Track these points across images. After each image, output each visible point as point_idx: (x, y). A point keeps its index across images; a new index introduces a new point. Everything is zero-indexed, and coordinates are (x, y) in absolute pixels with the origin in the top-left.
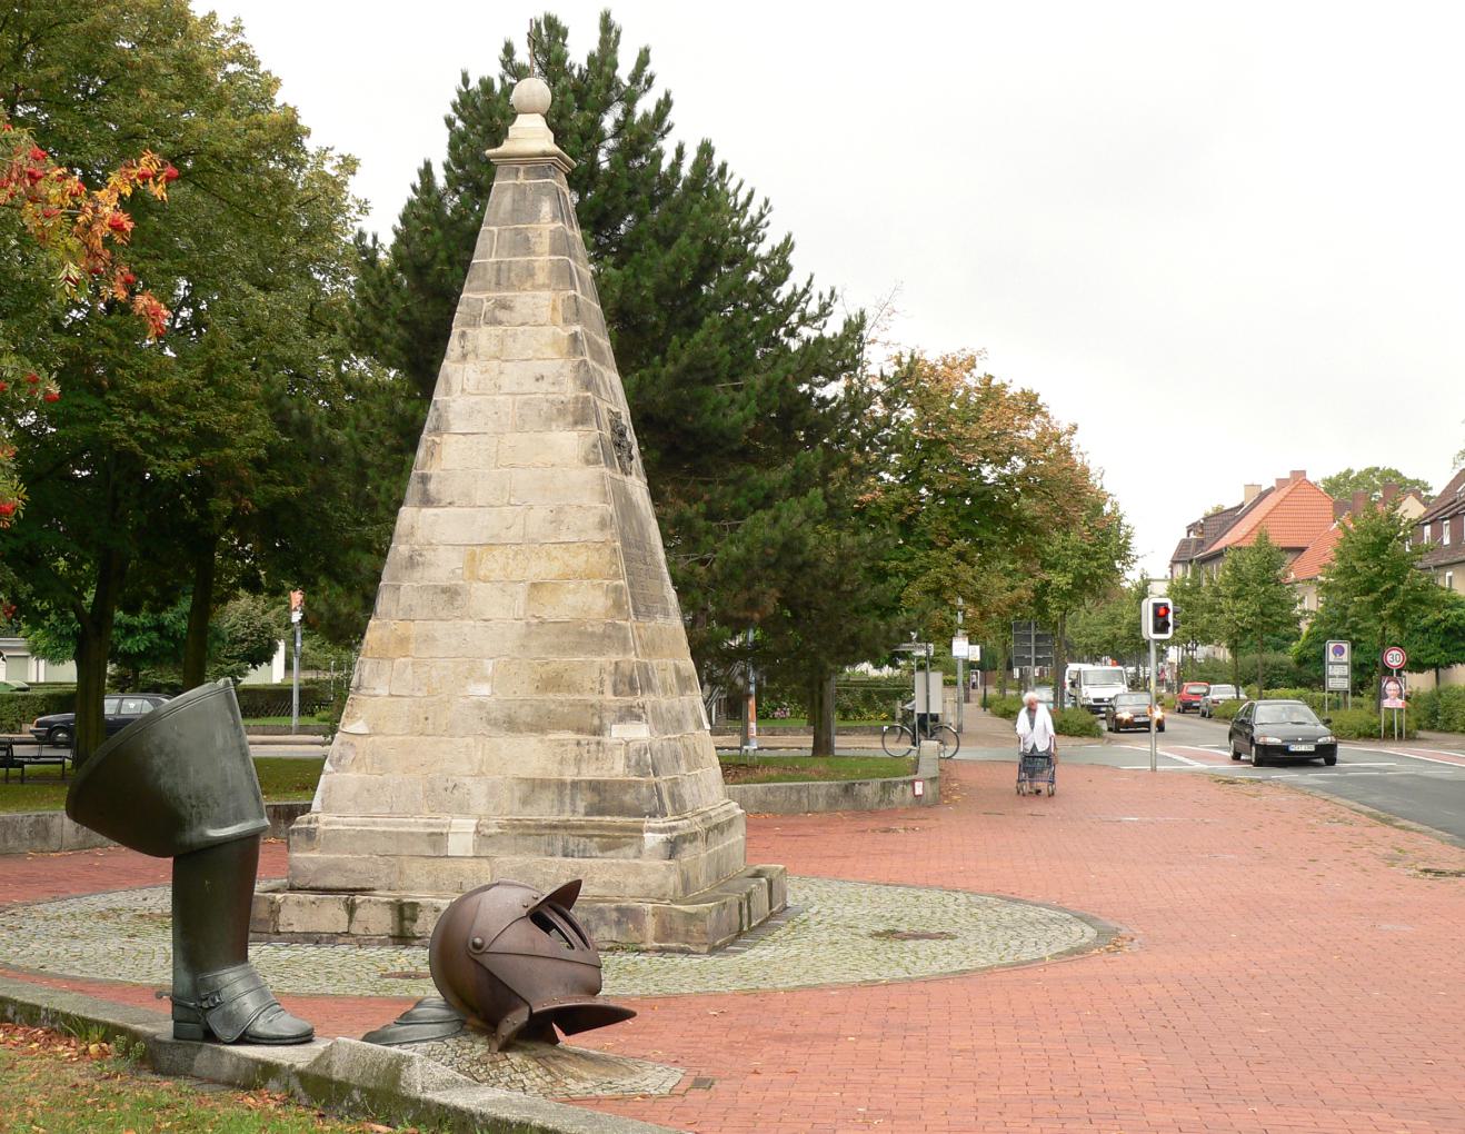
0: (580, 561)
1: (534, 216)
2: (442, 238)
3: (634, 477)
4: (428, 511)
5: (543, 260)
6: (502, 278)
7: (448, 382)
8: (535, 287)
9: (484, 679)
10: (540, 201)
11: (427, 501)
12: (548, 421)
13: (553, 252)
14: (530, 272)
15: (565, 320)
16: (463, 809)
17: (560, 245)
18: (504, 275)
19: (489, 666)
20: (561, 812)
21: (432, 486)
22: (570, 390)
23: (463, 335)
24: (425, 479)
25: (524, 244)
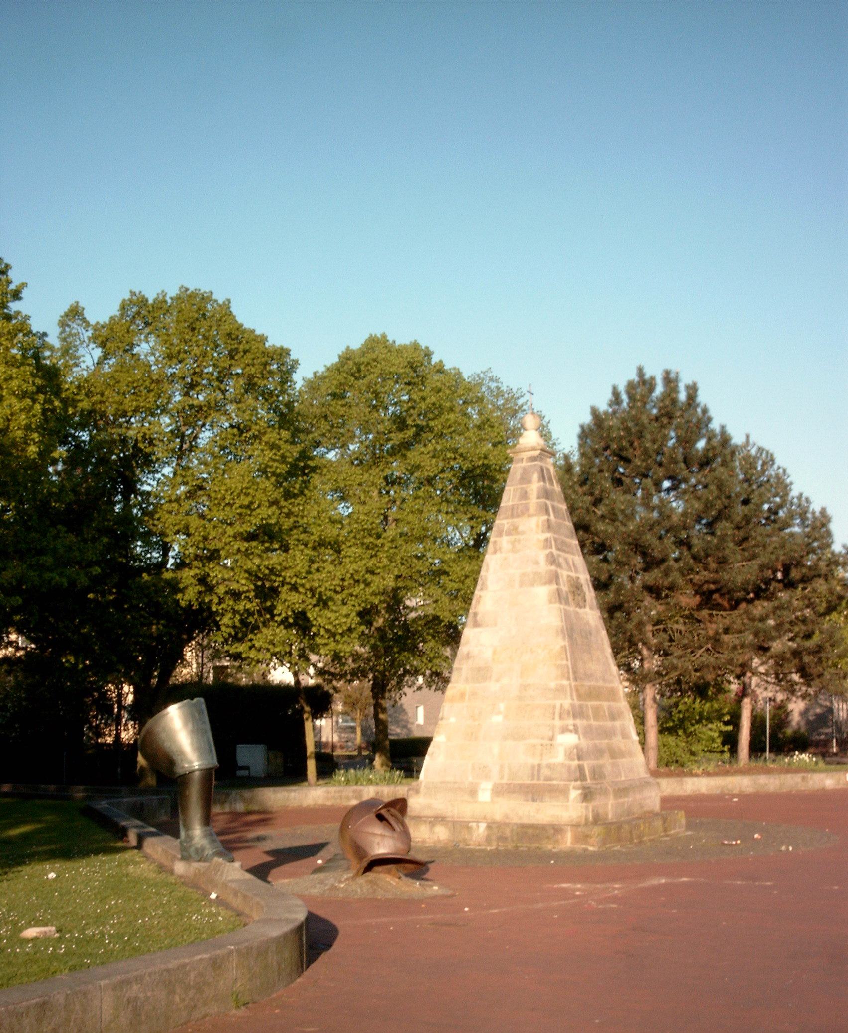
0: (217, 818)
1: (529, 482)
2: (772, 657)
3: (587, 609)
4: (477, 630)
5: (534, 501)
6: (514, 513)
7: (488, 566)
8: (529, 516)
9: (499, 713)
10: (807, 730)
11: (476, 624)
12: (532, 584)
13: (538, 498)
14: (526, 508)
15: (543, 532)
16: (487, 777)
17: (546, 494)
18: (515, 512)
19: (502, 706)
20: (533, 779)
21: (479, 617)
22: (544, 567)
23: (495, 542)
24: (475, 614)
25: (525, 495)
